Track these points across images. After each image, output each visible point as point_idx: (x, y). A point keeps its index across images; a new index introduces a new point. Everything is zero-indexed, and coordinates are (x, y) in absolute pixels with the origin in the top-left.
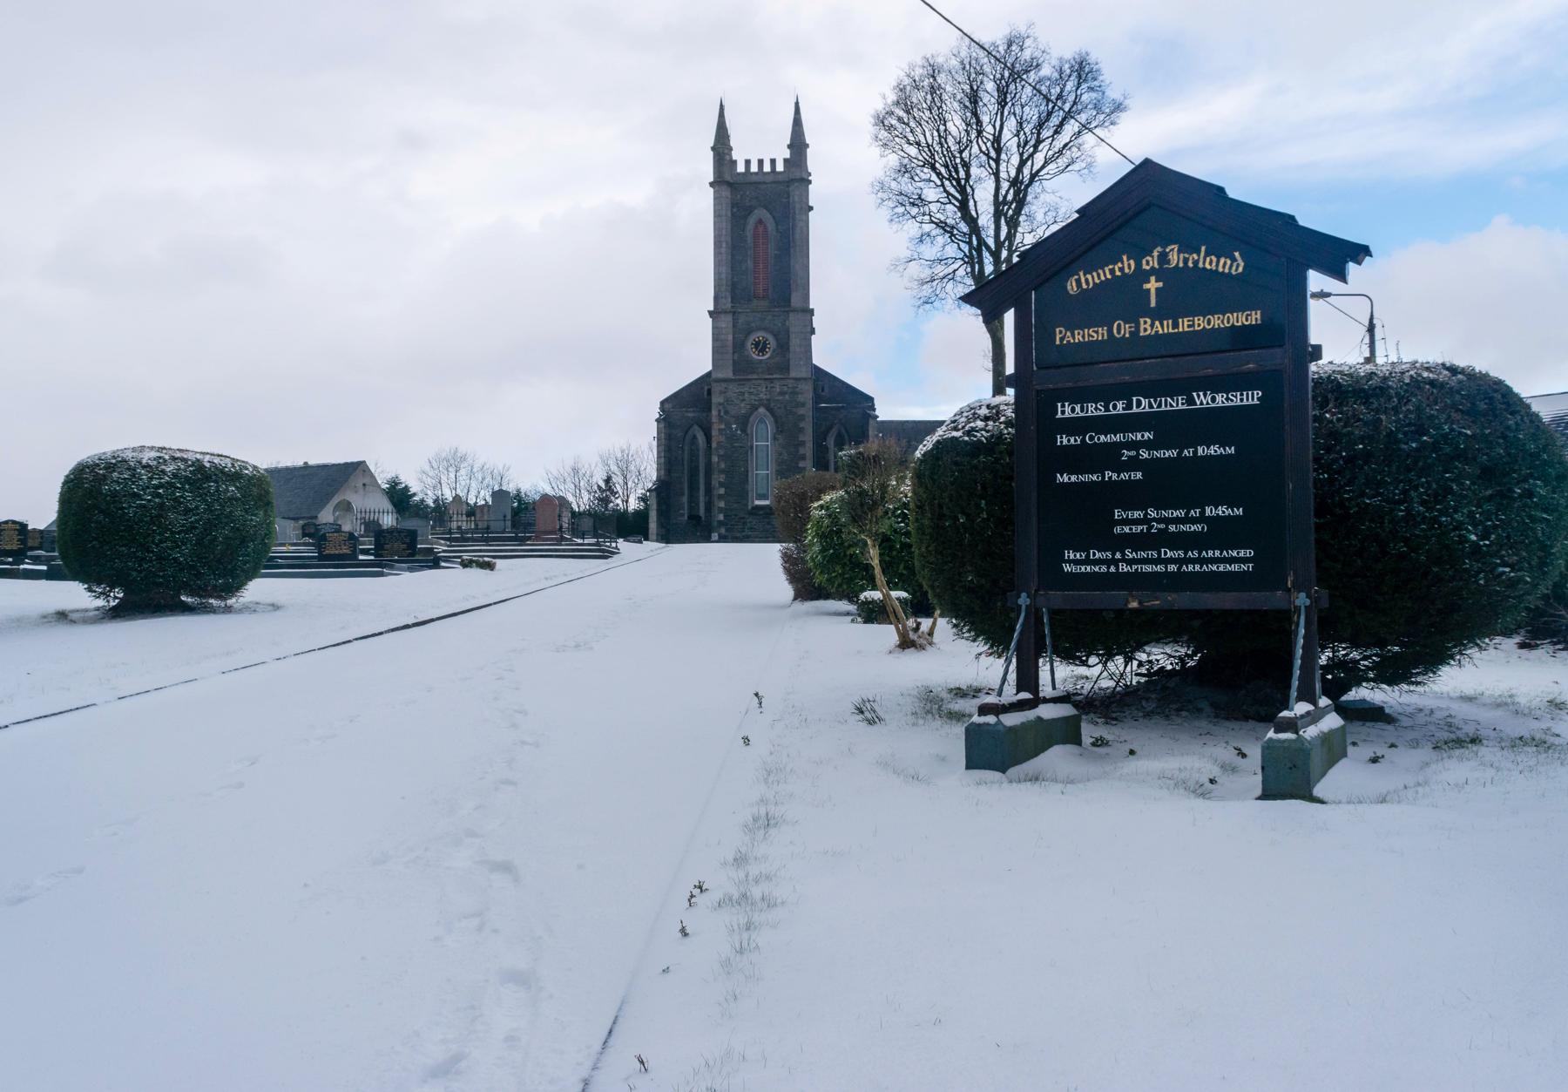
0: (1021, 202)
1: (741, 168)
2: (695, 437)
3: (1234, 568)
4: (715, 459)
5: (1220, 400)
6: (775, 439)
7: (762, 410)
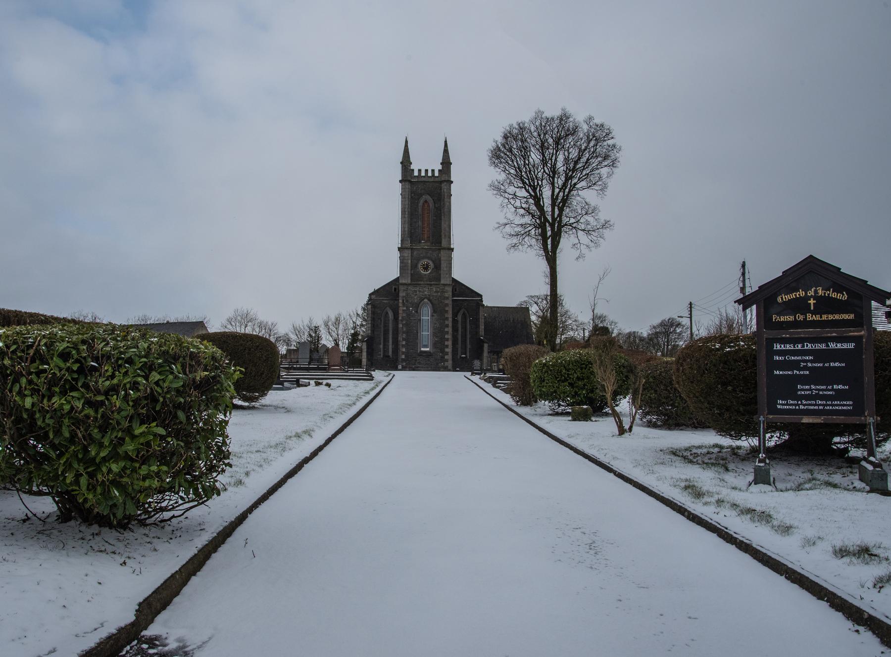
0: (565, 201)
1: (416, 174)
2: (387, 313)
3: (845, 408)
4: (400, 326)
6: (432, 316)
7: (426, 300)
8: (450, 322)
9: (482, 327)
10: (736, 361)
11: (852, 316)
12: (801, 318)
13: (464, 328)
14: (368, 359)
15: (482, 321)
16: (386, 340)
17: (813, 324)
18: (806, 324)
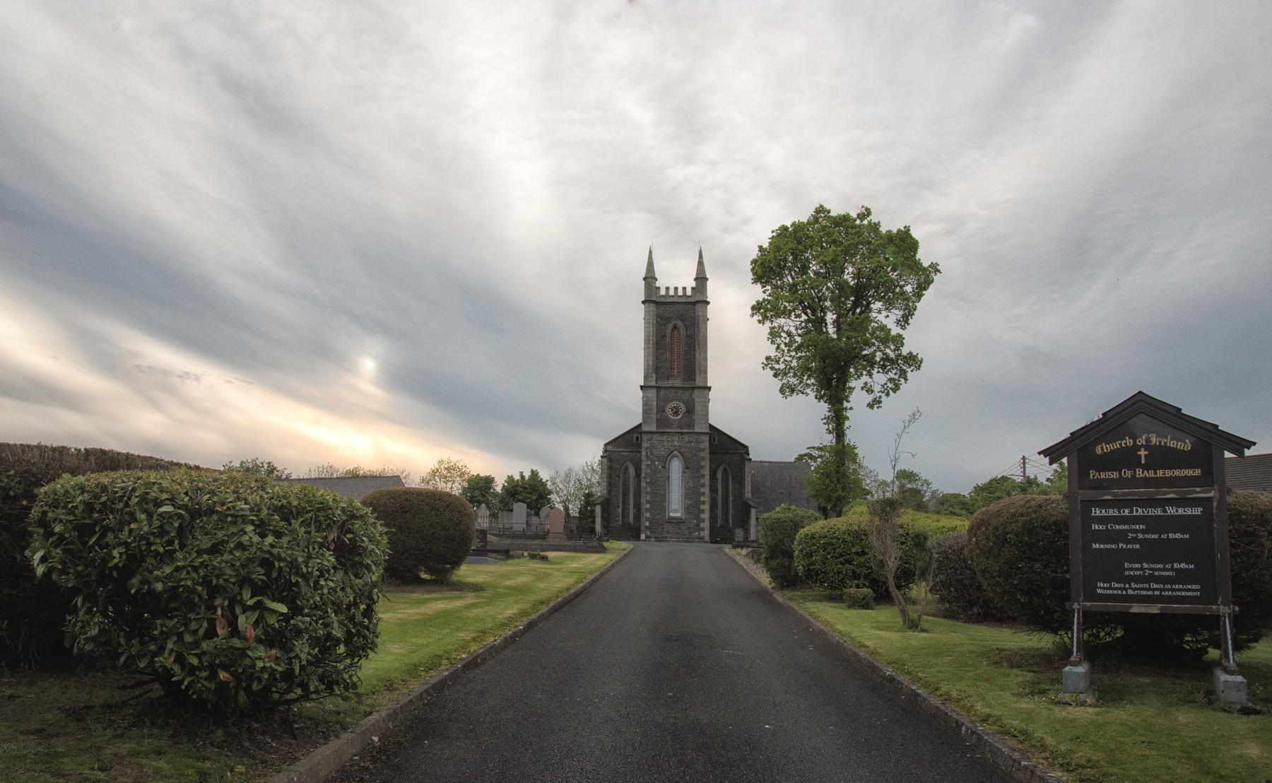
1: (663, 292)
3: (1190, 594)
4: (643, 484)
5: (1181, 511)
8: (706, 480)
9: (748, 488)
10: (1044, 528)
11: (1198, 472)
12: (1129, 474)
13: (726, 488)
14: (604, 527)
15: (748, 480)
16: (625, 503)
17: (1147, 482)
18: (1134, 482)
